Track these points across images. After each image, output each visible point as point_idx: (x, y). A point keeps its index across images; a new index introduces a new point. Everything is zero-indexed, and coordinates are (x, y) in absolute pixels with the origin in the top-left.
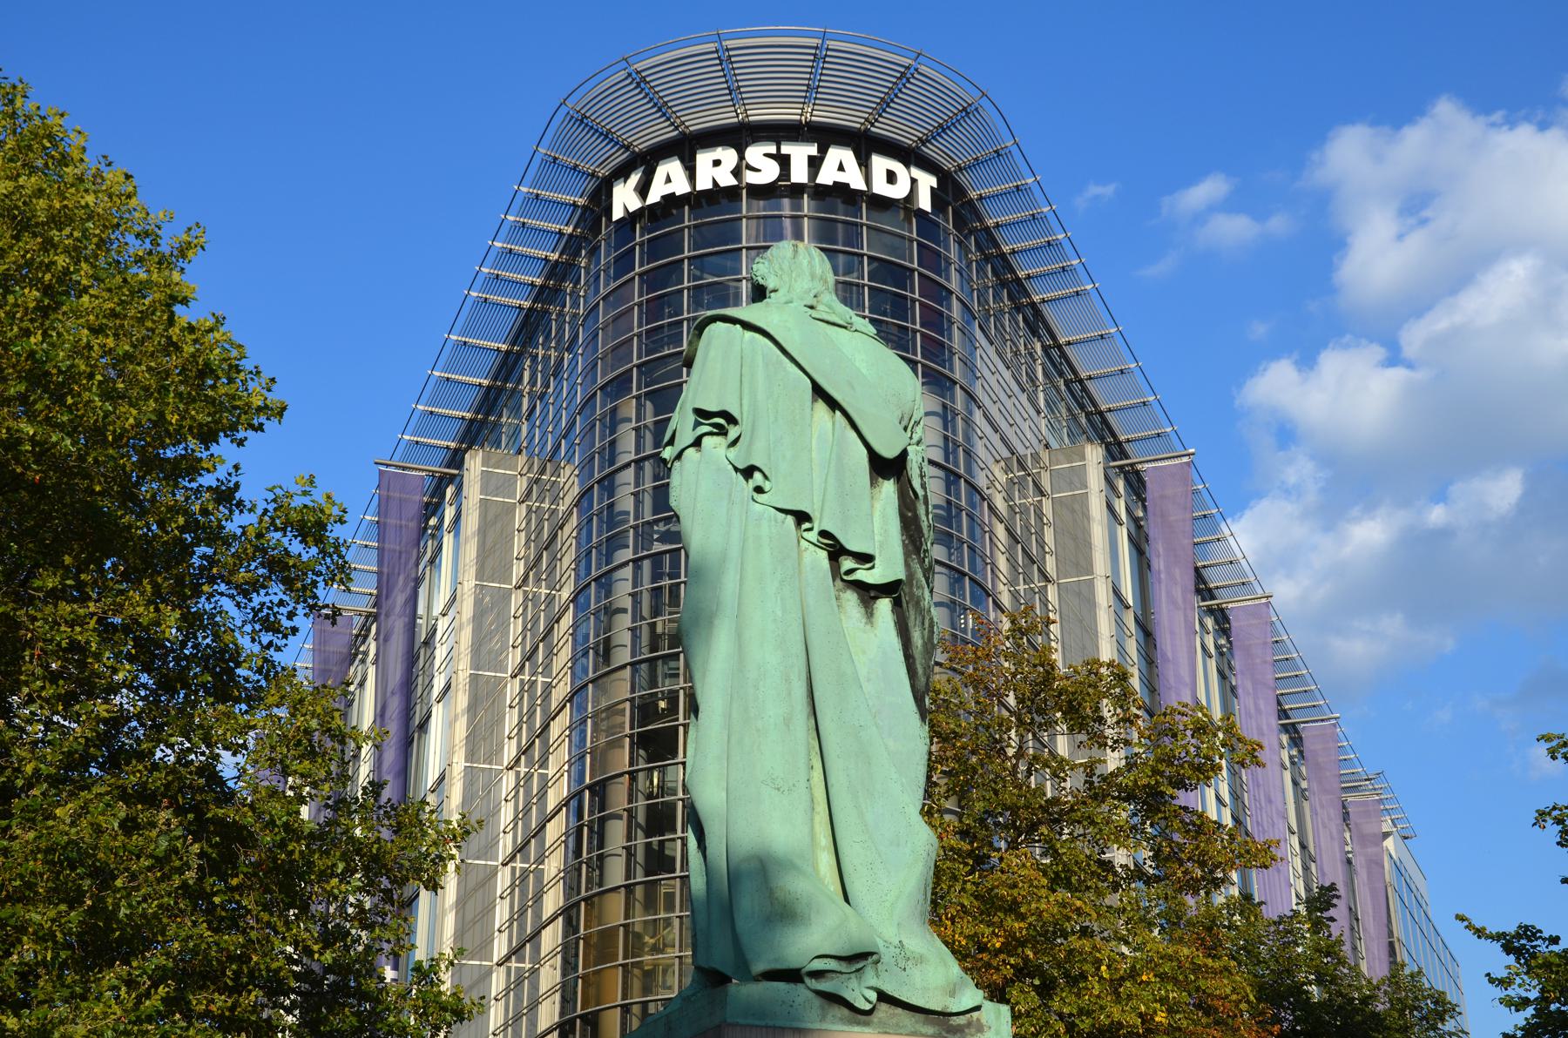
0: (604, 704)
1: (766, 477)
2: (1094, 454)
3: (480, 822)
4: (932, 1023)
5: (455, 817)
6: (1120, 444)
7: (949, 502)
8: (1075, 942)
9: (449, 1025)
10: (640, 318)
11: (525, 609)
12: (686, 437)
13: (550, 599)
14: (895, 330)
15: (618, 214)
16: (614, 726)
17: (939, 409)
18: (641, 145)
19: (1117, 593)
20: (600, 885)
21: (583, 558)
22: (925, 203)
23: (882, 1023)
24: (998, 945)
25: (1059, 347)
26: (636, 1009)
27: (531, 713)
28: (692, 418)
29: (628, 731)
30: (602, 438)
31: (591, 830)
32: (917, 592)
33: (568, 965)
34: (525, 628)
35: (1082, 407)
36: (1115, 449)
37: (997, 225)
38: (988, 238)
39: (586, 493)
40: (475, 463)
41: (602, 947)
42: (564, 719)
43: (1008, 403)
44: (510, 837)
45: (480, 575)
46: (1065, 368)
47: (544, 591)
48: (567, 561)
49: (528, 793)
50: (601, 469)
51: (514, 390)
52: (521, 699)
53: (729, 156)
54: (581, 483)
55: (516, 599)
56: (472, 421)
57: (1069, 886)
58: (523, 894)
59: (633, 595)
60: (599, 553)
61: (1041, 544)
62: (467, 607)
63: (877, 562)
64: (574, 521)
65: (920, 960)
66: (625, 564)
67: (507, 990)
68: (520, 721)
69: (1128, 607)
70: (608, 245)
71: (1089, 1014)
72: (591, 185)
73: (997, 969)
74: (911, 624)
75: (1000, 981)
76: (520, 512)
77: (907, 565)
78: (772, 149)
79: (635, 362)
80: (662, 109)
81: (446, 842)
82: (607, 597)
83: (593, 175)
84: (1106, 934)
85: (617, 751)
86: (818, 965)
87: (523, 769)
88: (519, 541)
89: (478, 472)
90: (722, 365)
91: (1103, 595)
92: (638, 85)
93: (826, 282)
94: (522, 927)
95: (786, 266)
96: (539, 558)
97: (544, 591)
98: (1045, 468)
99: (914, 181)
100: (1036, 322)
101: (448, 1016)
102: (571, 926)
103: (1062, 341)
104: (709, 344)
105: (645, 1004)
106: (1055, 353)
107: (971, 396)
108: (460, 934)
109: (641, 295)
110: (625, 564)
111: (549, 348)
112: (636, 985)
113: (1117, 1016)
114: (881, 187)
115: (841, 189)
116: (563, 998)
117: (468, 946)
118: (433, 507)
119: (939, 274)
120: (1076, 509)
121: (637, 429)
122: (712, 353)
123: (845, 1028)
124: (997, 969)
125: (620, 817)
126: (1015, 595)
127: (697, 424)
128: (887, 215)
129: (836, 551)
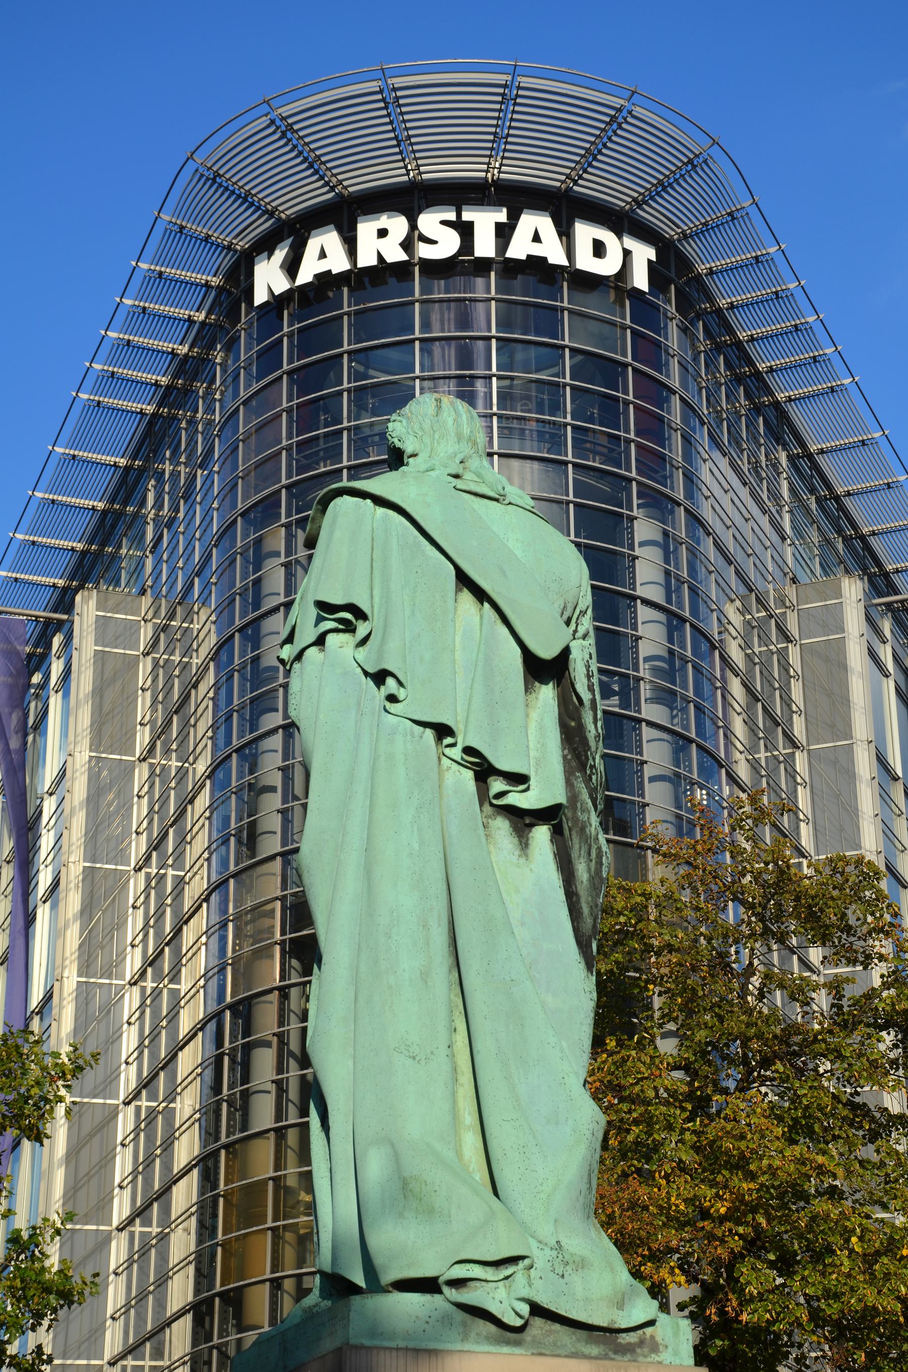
0: (249, 904)
1: (400, 684)
2: (852, 590)
3: (95, 1056)
4: (597, 1342)
5: (65, 1049)
6: (886, 575)
7: (671, 652)
8: (821, 1206)
9: (55, 1311)
10: (290, 428)
11: (152, 786)
12: (307, 634)
13: (182, 774)
14: (604, 440)
15: (260, 297)
16: (261, 932)
17: (659, 537)
18: (289, 211)
19: (882, 761)
20: (244, 1128)
21: (221, 724)
22: (640, 280)
23: (535, 1342)
24: (723, 1210)
25: (810, 456)
26: (288, 1285)
27: (160, 915)
28: (313, 612)
29: (278, 936)
30: (244, 576)
31: (233, 1061)
32: (582, 817)
33: (206, 1229)
34: (151, 810)
35: (840, 531)
36: (880, 582)
37: (732, 306)
38: (720, 322)
39: (225, 644)
40: (88, 608)
41: (247, 1206)
42: (200, 923)
43: (746, 529)
44: (133, 1068)
45: (95, 745)
46: (817, 482)
47: (175, 764)
48: (202, 726)
49: (155, 1013)
50: (244, 614)
51: (136, 515)
52: (148, 897)
53: (398, 225)
54: (219, 632)
55: (141, 774)
56: (84, 553)
57: (810, 1133)
58: (150, 1139)
59: (284, 769)
60: (242, 718)
61: (787, 701)
62: (79, 788)
63: (532, 782)
64: (211, 678)
65: (582, 1264)
66: (274, 731)
67: (130, 1261)
68: (146, 925)
69: (896, 779)
70: (249, 336)
71: (837, 1296)
72: (227, 261)
73: (722, 1241)
74: (574, 854)
75: (725, 1256)
76: (145, 667)
77: (569, 783)
78: (452, 216)
79: (284, 481)
80: (313, 164)
81: (53, 1081)
82: (251, 772)
83: (229, 248)
84: (858, 1196)
85: (265, 962)
86: (460, 1272)
87: (150, 984)
88: (143, 702)
89: (92, 619)
90: (351, 546)
91: (864, 764)
92: (284, 135)
93: (475, 443)
94: (148, 1182)
95: (427, 425)
96: (168, 723)
97: (175, 764)
98: (792, 608)
99: (627, 253)
100: (779, 425)
101: (53, 1300)
102: (209, 1179)
103: (813, 448)
104: (334, 521)
105: (299, 1277)
106: (804, 464)
107: (695, 519)
108: (72, 1191)
109: (290, 400)
110: (274, 731)
111: (179, 463)
112: (289, 1254)
113: (871, 1300)
114: (586, 262)
115: (536, 264)
116: (198, 1270)
117: (81, 1210)
118: (38, 661)
119: (644, 389)
120: (833, 660)
121: (287, 565)
122: (337, 534)
123: (492, 1349)
124: (722, 1241)
125: (268, 1044)
126: (754, 765)
127: (319, 620)
128: (594, 297)
129: (484, 771)
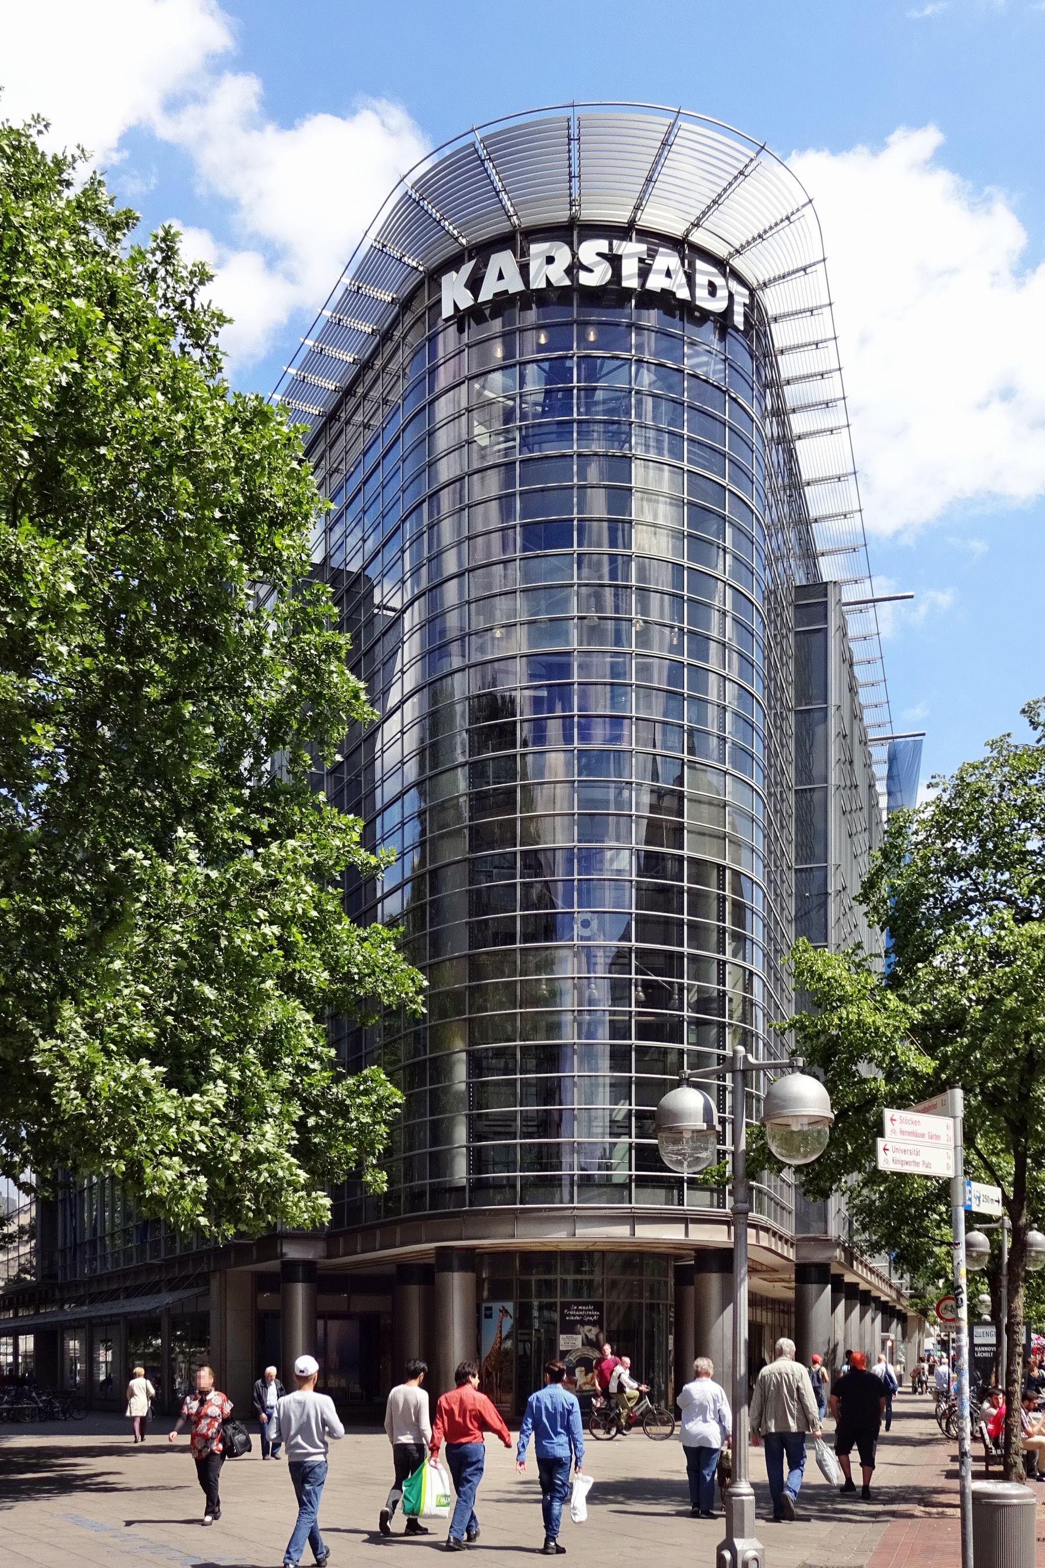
53: (563, 255)
